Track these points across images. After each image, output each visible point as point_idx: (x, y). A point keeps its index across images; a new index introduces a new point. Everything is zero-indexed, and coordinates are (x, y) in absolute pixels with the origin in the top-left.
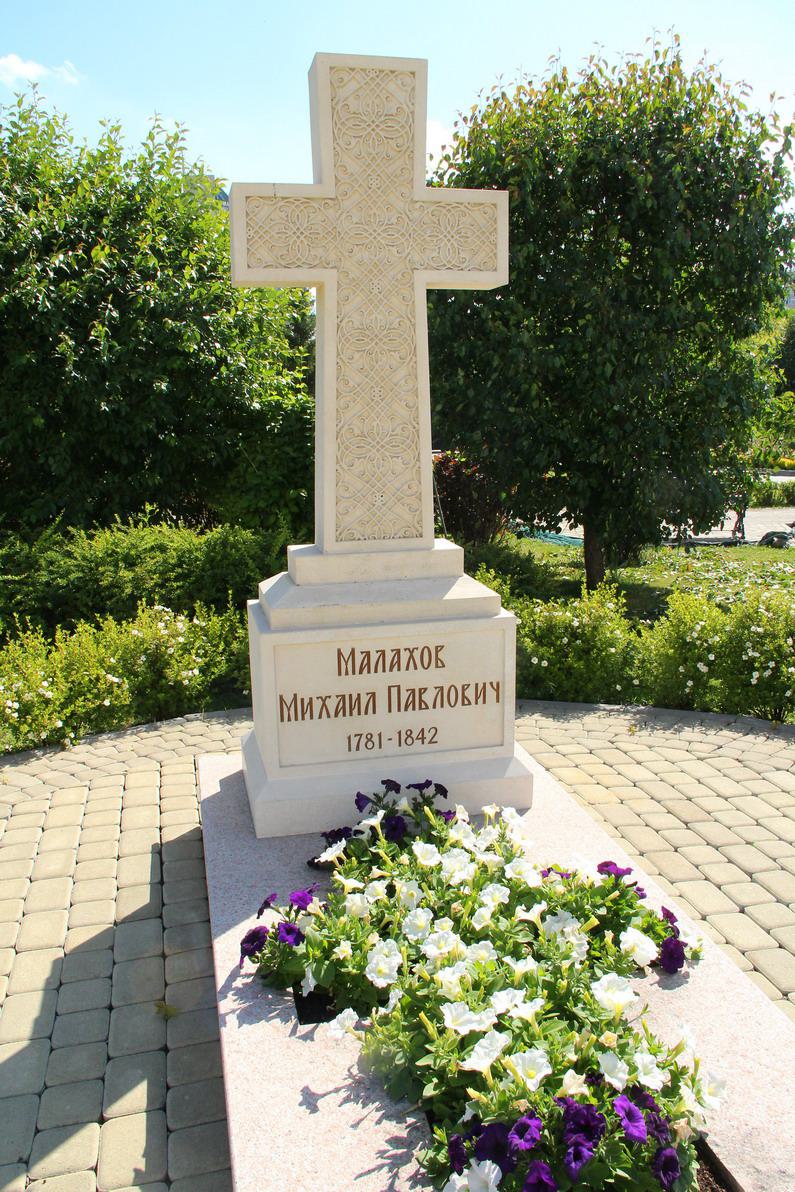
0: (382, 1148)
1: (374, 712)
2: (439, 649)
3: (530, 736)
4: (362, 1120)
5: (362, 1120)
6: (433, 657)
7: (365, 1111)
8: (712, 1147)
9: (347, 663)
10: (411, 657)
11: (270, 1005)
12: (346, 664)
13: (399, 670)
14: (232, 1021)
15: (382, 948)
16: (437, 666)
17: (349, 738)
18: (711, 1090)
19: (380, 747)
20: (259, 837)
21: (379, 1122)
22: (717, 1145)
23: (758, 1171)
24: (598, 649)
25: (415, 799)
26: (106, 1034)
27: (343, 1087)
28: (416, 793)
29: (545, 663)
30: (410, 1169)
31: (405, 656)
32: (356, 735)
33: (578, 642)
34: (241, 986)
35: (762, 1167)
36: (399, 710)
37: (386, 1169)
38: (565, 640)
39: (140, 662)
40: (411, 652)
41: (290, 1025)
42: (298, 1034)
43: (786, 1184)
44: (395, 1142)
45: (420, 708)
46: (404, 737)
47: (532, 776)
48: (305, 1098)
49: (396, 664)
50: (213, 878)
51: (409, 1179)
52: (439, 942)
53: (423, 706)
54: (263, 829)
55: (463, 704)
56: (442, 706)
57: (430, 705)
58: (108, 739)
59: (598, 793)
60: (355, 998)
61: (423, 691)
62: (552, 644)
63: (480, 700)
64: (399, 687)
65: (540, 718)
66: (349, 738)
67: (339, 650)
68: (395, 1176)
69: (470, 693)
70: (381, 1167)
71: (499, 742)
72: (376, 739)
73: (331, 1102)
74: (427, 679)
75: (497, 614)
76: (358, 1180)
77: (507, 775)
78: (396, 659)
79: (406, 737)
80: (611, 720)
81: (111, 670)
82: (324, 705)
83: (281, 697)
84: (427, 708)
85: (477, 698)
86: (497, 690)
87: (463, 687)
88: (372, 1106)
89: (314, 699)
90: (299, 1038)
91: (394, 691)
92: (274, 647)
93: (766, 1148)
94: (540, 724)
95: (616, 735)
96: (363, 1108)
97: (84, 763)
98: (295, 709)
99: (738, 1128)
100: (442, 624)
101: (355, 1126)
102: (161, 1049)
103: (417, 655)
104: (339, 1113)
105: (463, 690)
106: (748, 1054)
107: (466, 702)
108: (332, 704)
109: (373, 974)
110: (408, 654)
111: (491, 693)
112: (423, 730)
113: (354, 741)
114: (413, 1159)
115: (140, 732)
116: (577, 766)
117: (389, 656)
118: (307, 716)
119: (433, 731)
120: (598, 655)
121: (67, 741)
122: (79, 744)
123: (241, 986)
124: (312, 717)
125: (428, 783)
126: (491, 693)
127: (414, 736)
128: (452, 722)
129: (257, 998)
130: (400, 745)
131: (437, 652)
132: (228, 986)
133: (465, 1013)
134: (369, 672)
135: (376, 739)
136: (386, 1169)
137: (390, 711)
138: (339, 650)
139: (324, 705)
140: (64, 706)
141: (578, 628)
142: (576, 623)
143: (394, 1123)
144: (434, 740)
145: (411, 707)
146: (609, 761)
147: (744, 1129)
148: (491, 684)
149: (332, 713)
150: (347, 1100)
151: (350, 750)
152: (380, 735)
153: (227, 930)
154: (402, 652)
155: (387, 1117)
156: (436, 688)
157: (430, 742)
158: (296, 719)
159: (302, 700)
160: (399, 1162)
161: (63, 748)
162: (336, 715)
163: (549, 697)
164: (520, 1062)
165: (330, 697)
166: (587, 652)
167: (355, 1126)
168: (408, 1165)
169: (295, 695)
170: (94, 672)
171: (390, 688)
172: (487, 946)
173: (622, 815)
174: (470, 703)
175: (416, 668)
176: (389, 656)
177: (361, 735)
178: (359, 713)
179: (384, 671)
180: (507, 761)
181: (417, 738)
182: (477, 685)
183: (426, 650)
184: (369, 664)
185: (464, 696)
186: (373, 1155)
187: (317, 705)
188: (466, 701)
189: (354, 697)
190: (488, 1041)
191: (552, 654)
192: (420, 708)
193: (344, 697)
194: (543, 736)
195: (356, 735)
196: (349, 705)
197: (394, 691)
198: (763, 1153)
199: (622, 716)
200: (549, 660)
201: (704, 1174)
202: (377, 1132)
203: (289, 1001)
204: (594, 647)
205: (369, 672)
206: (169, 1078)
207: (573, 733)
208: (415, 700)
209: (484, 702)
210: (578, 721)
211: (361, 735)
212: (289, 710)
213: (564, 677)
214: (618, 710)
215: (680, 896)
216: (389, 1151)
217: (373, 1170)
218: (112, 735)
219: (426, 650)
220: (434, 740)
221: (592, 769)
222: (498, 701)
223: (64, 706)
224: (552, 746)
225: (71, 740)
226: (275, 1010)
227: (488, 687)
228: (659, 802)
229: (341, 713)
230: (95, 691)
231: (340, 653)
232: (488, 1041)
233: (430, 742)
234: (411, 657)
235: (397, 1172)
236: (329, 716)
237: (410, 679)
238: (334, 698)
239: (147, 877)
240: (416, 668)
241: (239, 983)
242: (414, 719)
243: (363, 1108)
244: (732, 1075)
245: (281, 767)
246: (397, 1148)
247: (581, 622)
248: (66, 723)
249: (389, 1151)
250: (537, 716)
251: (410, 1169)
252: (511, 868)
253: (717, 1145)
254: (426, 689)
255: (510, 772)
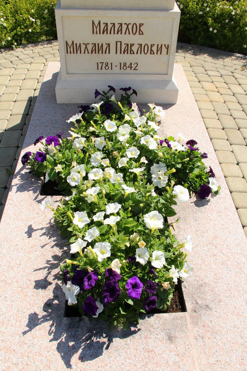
0: (49, 260)
1: (109, 53)
2: (141, 25)
3: (199, 65)
4: (46, 244)
5: (46, 244)
6: (138, 29)
7: (49, 241)
8: (183, 288)
9: (98, 28)
10: (127, 28)
11: (32, 184)
12: (96, 29)
13: (121, 33)
14: (14, 189)
15: (77, 168)
16: (139, 34)
17: (98, 64)
18: (186, 270)
19: (112, 69)
20: (58, 103)
21: (52, 247)
22: (185, 287)
23: (197, 303)
24: (240, 27)
25: (122, 95)
26: (12, 164)
27: (45, 228)
28: (123, 92)
29: (215, 31)
30: (55, 271)
31: (124, 27)
32: (101, 63)
33: (232, 23)
34: (24, 173)
35: (200, 302)
36: (121, 53)
37: (47, 269)
38: (227, 21)
39: (45, 13)
40: (128, 25)
41: (36, 195)
42: (37, 200)
43: (206, 312)
44: (55, 257)
45: (131, 53)
46: (122, 66)
47: (178, 90)
48: (28, 230)
49: (120, 31)
50: (33, 120)
51: (54, 276)
52: (96, 173)
53: (132, 52)
54: (59, 101)
55: (151, 53)
56: (141, 53)
57: (135, 52)
58: (31, 46)
59: (216, 96)
60: (65, 186)
61: (132, 45)
62: (221, 22)
63: (159, 52)
64: (121, 42)
65: (207, 56)
66: (98, 64)
67: (93, 21)
68: (49, 273)
69: (155, 49)
70: (45, 268)
71: (166, 73)
72: (110, 65)
73: (38, 234)
74: (135, 39)
75: (172, 9)
76: (36, 272)
77: (167, 88)
78: (120, 29)
79: (123, 66)
80: (236, 62)
81: (32, 16)
82: (86, 47)
83: (66, 42)
84: (134, 53)
85: (157, 51)
86: (167, 49)
87: (151, 45)
88: (53, 239)
89: (82, 45)
90: (36, 201)
91: (119, 44)
92: (62, 16)
93: (206, 293)
94: (206, 59)
95: (236, 69)
96: (49, 239)
97: (18, 57)
98: (72, 48)
99: (198, 281)
100: (143, 13)
101: (42, 247)
102: (4, 188)
103: (130, 27)
104: (39, 239)
105: (151, 47)
106: (219, 246)
107: (152, 53)
108: (90, 47)
109: (70, 180)
110: (126, 26)
111: (164, 50)
112: (131, 64)
113: (100, 65)
114: (59, 267)
115: (44, 44)
116: (212, 82)
117: (117, 26)
118: (79, 52)
119: (136, 64)
120: (240, 30)
121: (14, 46)
122: (19, 48)
123: (24, 173)
124: (81, 53)
125: (130, 89)
126: (164, 50)
127: (127, 65)
128: (145, 61)
129: (28, 180)
130: (120, 69)
131: (140, 27)
132: (19, 173)
133: (85, 217)
134: (107, 33)
135: (110, 65)
136: (47, 269)
137: (116, 53)
138: (93, 21)
139: (86, 47)
140: (12, 30)
141: (234, 15)
142: (233, 13)
143: (58, 248)
144: (136, 69)
145: (126, 52)
146: (227, 82)
147: (201, 282)
148: (165, 45)
149: (90, 52)
150: (44, 234)
151: (98, 69)
152: (111, 64)
153: (29, 146)
154: (123, 25)
155: (56, 245)
156: (138, 44)
157: (134, 69)
158: (74, 53)
159: (76, 44)
160: (53, 267)
161: (13, 49)
162: (92, 52)
163: (215, 47)
164: (100, 246)
165: (89, 44)
166: (235, 28)
167: (42, 247)
168: (56, 269)
169: (73, 42)
170: (26, 16)
171: (117, 42)
172: (120, 175)
173: (222, 109)
174: (154, 53)
175: (129, 34)
176: (117, 26)
177: (103, 63)
178: (102, 53)
179: (114, 33)
180: (169, 81)
181: (128, 67)
182: (158, 45)
183: (135, 25)
184: (107, 29)
185: (151, 50)
186: (45, 262)
187: (83, 47)
188: (152, 52)
189: (100, 45)
190: (93, 231)
191: (219, 27)
192: (131, 53)
193: (95, 44)
194: (204, 66)
195: (101, 63)
196: (97, 49)
197: (119, 44)
198: (203, 295)
199: (242, 61)
200: (217, 30)
201: (175, 297)
202: (50, 251)
203: (40, 183)
204: (239, 26)
205: (107, 33)
206: (2, 200)
207: (217, 66)
208: (128, 49)
209: (161, 54)
210: (222, 60)
211: (103, 63)
212: (70, 48)
213: (222, 39)
214: (241, 57)
215: (232, 152)
216: (51, 261)
217: (42, 269)
218: (33, 45)
219: (135, 25)
220: (136, 69)
221: (218, 84)
222: (167, 54)
223: (12, 30)
224: (206, 71)
225: (16, 46)
226: (33, 186)
227: (163, 46)
228: (241, 105)
229: (94, 52)
230: (25, 25)
231: (93, 23)
232: (93, 231)
233: (134, 69)
234: (127, 28)
235: (51, 272)
236: (88, 53)
237: (126, 39)
238: (90, 44)
239: (22, 112)
240: (129, 34)
241: (23, 172)
242: (127, 58)
243: (49, 239)
244: (207, 255)
245: (67, 74)
246: (55, 260)
247: (236, 13)
248: (13, 37)
249: (51, 261)
250: (206, 55)
251: (55, 271)
252: (144, 139)
253: (185, 287)
254: (133, 44)
255: (169, 87)
